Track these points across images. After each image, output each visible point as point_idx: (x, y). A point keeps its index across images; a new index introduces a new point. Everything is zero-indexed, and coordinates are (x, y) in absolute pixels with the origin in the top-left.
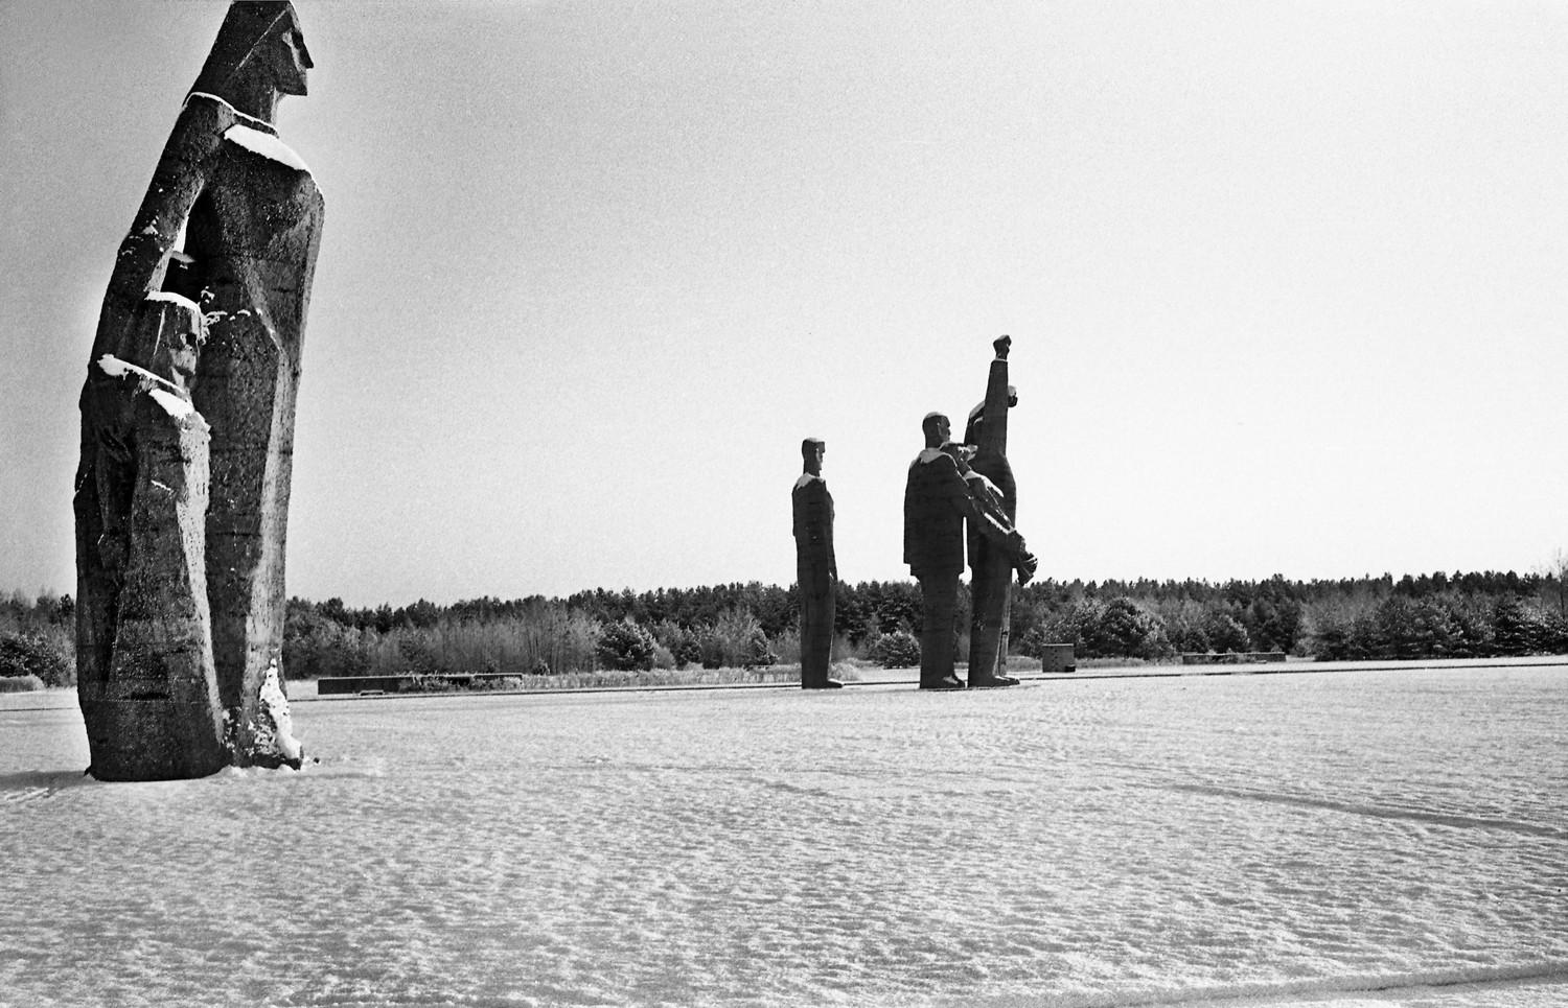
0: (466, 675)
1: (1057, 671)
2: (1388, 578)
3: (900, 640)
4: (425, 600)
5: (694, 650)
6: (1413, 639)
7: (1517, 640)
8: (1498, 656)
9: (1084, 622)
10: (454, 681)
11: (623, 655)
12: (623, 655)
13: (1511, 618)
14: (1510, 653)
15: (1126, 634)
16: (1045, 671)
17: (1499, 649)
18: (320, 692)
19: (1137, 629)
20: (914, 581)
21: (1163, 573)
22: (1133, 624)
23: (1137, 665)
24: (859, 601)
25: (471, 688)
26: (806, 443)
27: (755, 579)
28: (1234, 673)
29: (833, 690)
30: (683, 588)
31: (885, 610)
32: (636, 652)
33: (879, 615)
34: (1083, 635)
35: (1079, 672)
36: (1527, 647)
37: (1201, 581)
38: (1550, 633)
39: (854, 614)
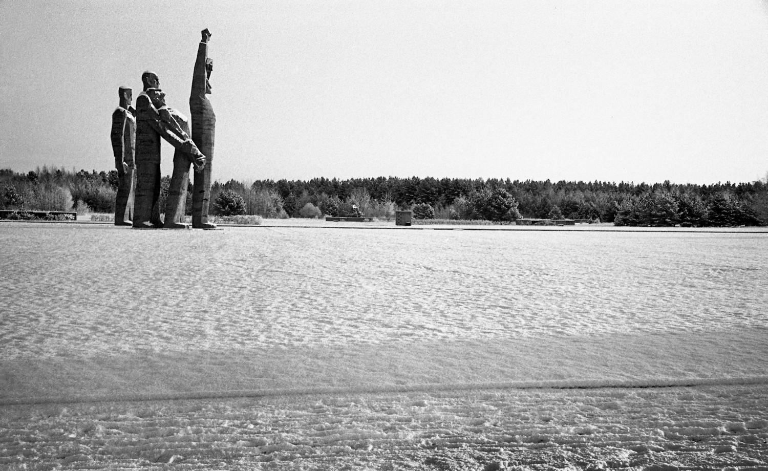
0: (44, 212)
1: (401, 225)
2: (548, 182)
3: (424, 208)
4: (234, 179)
5: (333, 209)
6: (655, 216)
7: (722, 219)
8: (747, 225)
9: (478, 201)
10: (36, 214)
11: (224, 208)
12: (224, 208)
13: (720, 206)
14: (715, 225)
15: (499, 208)
16: (397, 224)
17: (713, 223)
18: (397, 224)
19: (505, 206)
20: (116, 170)
21: (588, 178)
22: (503, 203)
23: (489, 224)
24: (436, 188)
25: (46, 219)
26: (120, 88)
27: (562, 179)
28: (452, 229)
29: (126, 227)
30: (289, 179)
31: (450, 193)
32: (231, 207)
33: (446, 195)
34: (476, 207)
35: (412, 226)
36: (727, 222)
37: (630, 183)
38: (743, 215)
39: (432, 194)
